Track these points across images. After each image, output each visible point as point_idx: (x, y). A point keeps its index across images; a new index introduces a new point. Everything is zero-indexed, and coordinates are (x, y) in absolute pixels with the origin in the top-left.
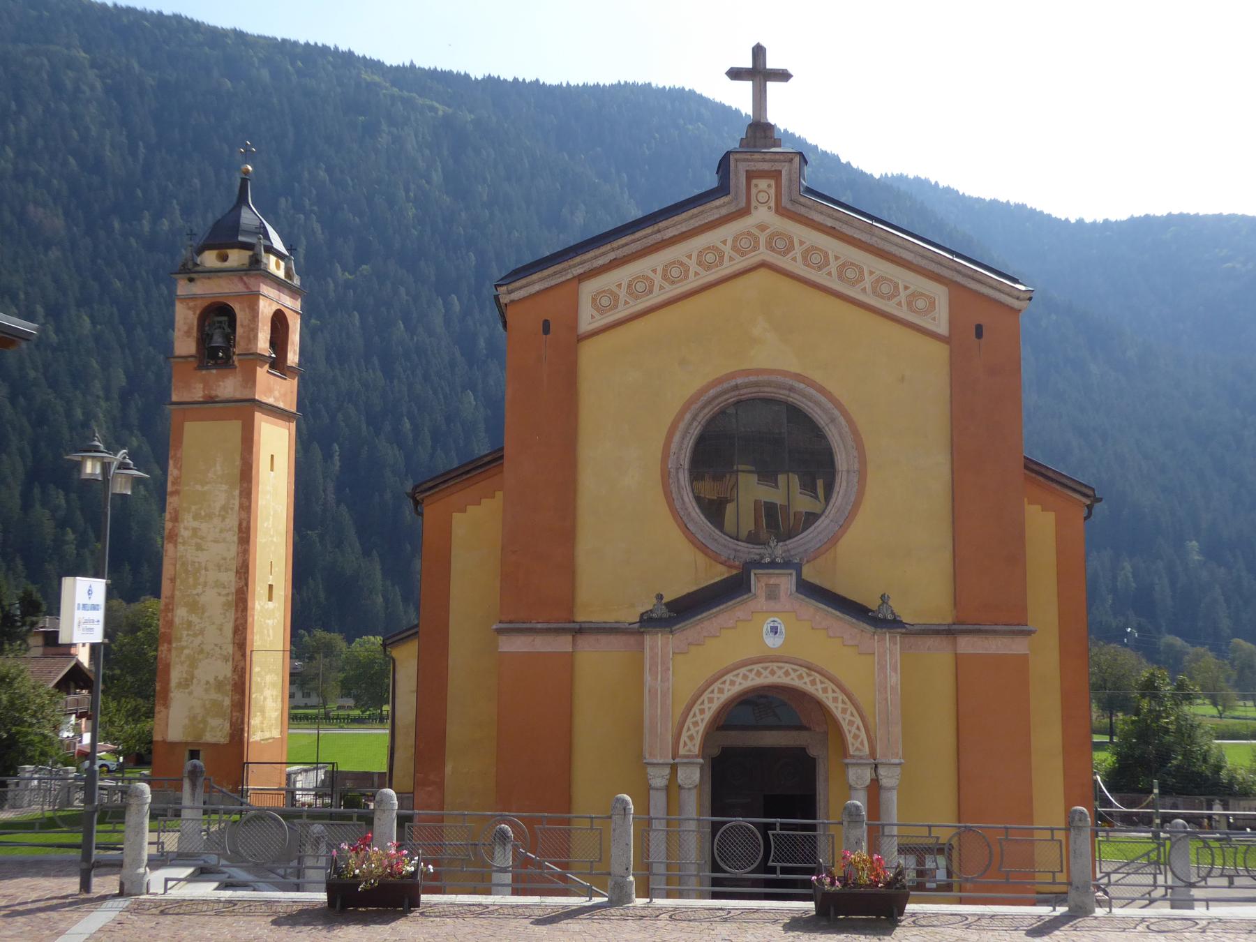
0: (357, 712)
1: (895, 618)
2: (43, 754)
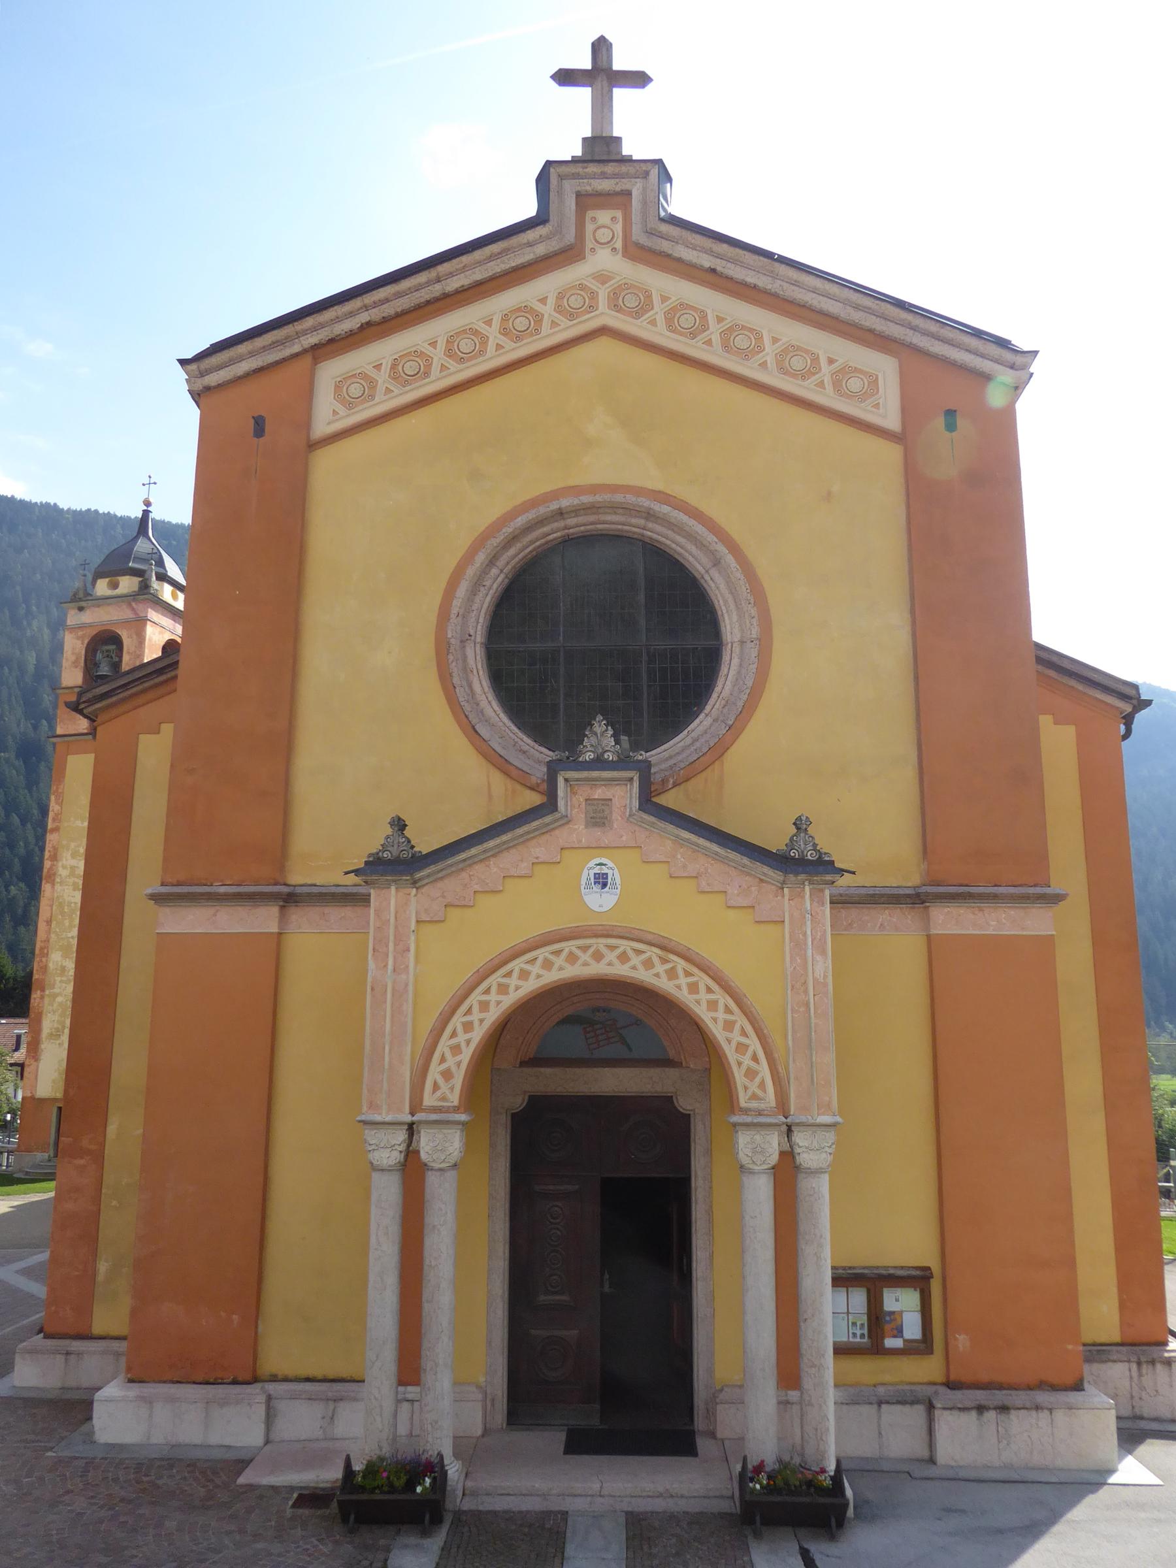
1: (820, 857)
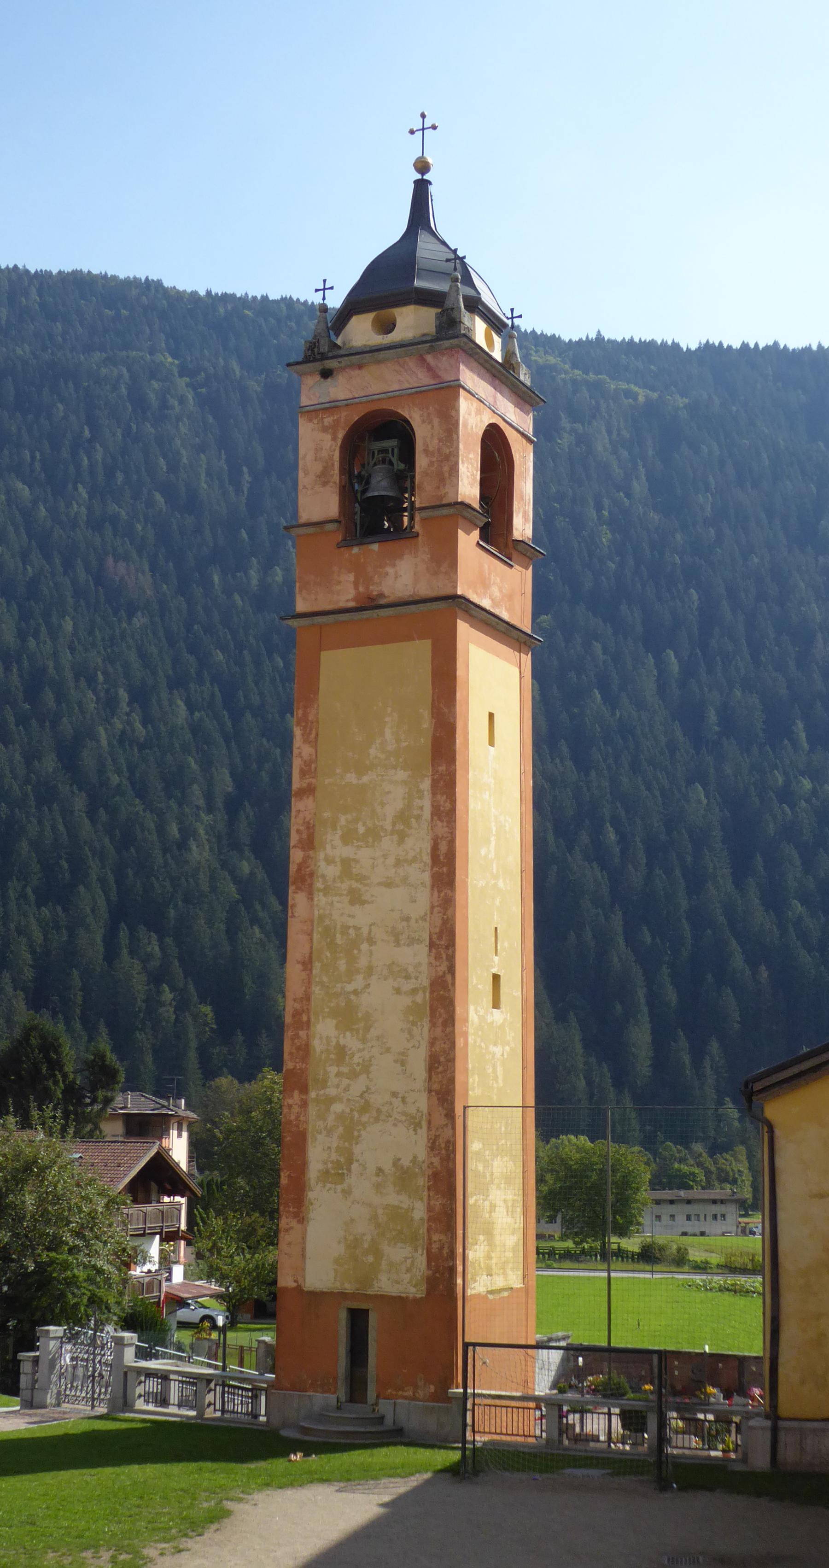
0: (569, 1244)
2: (94, 1301)
